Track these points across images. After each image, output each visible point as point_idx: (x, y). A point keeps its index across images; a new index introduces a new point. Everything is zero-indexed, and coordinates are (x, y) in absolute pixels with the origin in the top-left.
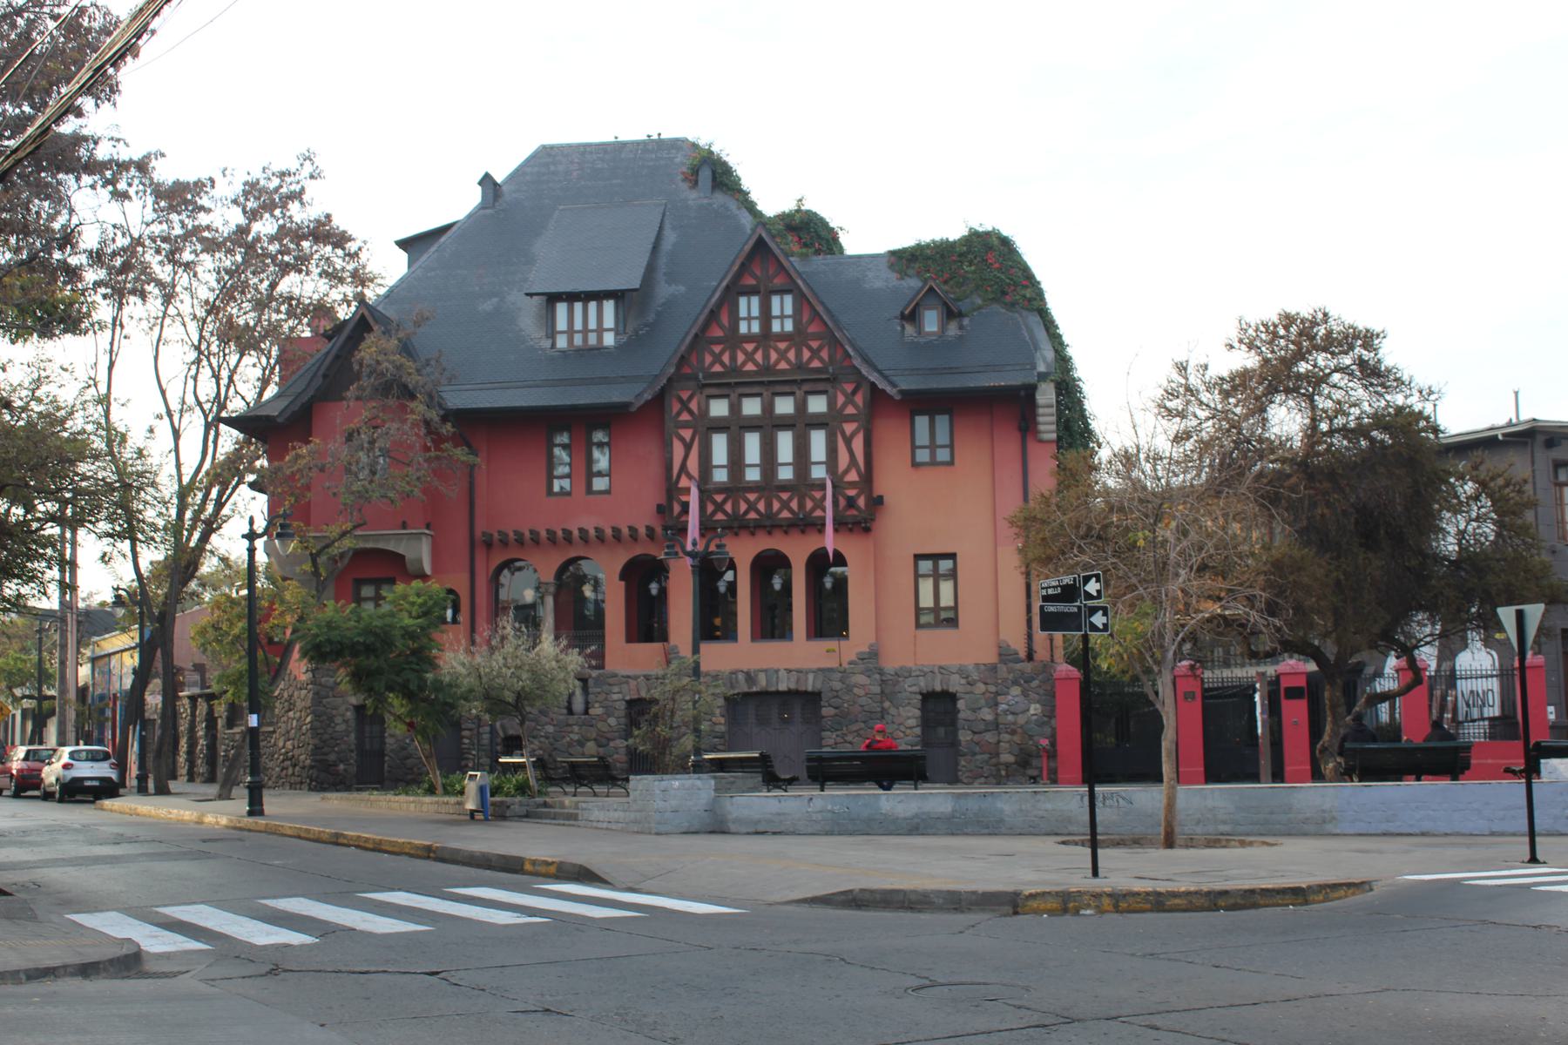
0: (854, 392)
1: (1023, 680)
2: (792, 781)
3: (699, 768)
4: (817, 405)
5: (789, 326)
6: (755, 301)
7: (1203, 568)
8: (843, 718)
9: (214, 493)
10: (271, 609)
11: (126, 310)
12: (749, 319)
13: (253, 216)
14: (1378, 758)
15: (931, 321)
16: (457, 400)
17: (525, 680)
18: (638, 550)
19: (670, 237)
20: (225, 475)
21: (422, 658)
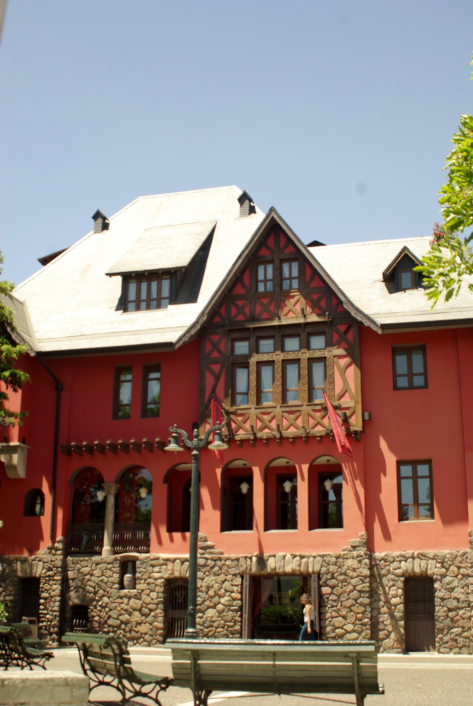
0: (346, 332)
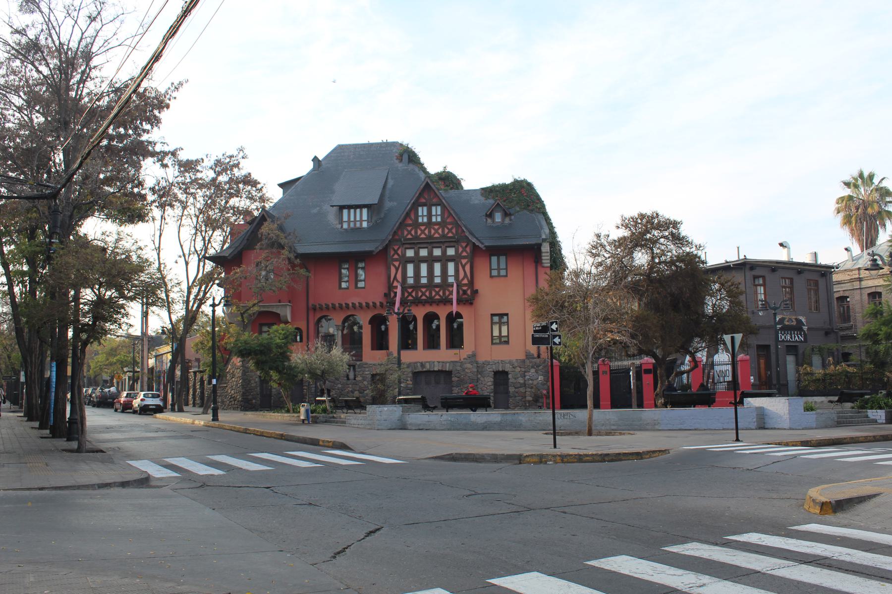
1: (536, 366)
2: (435, 408)
3: (394, 402)
4: (451, 252)
5: (439, 219)
6: (425, 209)
7: (605, 320)
8: (461, 382)
9: (203, 288)
10: (224, 335)
11: (166, 213)
12: (423, 216)
13: (219, 174)
14: (680, 399)
15: (498, 217)
16: (302, 249)
17: (325, 366)
18: (376, 312)
19: (391, 183)
20: (207, 280)
21: (285, 356)
